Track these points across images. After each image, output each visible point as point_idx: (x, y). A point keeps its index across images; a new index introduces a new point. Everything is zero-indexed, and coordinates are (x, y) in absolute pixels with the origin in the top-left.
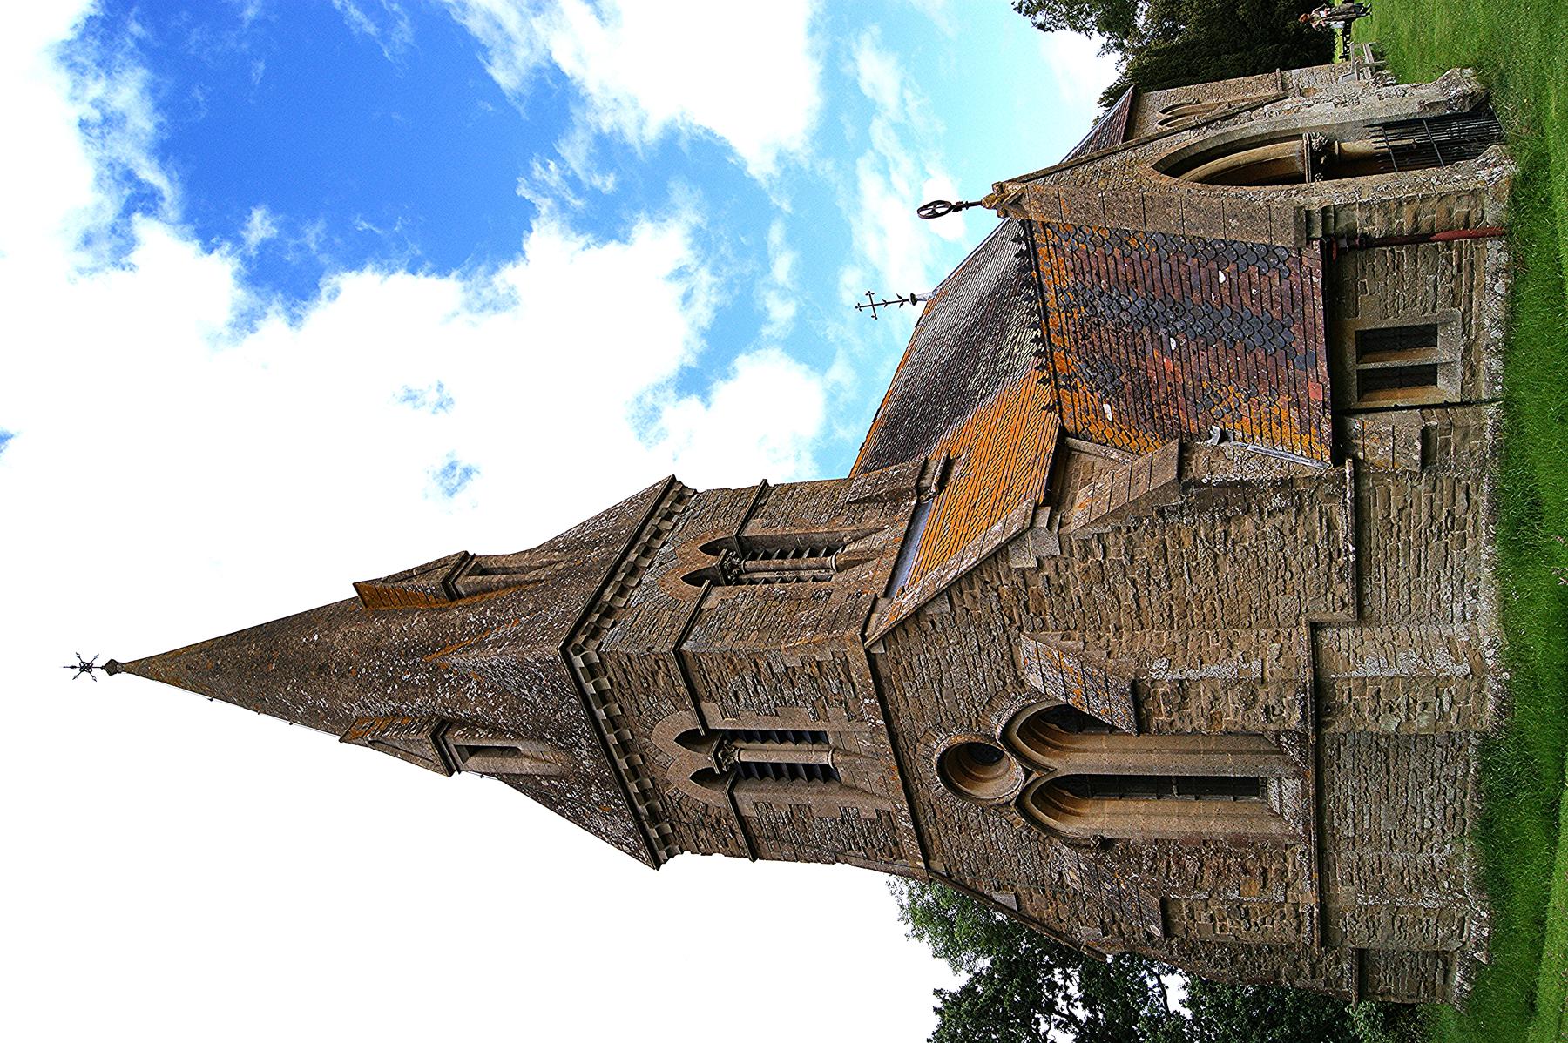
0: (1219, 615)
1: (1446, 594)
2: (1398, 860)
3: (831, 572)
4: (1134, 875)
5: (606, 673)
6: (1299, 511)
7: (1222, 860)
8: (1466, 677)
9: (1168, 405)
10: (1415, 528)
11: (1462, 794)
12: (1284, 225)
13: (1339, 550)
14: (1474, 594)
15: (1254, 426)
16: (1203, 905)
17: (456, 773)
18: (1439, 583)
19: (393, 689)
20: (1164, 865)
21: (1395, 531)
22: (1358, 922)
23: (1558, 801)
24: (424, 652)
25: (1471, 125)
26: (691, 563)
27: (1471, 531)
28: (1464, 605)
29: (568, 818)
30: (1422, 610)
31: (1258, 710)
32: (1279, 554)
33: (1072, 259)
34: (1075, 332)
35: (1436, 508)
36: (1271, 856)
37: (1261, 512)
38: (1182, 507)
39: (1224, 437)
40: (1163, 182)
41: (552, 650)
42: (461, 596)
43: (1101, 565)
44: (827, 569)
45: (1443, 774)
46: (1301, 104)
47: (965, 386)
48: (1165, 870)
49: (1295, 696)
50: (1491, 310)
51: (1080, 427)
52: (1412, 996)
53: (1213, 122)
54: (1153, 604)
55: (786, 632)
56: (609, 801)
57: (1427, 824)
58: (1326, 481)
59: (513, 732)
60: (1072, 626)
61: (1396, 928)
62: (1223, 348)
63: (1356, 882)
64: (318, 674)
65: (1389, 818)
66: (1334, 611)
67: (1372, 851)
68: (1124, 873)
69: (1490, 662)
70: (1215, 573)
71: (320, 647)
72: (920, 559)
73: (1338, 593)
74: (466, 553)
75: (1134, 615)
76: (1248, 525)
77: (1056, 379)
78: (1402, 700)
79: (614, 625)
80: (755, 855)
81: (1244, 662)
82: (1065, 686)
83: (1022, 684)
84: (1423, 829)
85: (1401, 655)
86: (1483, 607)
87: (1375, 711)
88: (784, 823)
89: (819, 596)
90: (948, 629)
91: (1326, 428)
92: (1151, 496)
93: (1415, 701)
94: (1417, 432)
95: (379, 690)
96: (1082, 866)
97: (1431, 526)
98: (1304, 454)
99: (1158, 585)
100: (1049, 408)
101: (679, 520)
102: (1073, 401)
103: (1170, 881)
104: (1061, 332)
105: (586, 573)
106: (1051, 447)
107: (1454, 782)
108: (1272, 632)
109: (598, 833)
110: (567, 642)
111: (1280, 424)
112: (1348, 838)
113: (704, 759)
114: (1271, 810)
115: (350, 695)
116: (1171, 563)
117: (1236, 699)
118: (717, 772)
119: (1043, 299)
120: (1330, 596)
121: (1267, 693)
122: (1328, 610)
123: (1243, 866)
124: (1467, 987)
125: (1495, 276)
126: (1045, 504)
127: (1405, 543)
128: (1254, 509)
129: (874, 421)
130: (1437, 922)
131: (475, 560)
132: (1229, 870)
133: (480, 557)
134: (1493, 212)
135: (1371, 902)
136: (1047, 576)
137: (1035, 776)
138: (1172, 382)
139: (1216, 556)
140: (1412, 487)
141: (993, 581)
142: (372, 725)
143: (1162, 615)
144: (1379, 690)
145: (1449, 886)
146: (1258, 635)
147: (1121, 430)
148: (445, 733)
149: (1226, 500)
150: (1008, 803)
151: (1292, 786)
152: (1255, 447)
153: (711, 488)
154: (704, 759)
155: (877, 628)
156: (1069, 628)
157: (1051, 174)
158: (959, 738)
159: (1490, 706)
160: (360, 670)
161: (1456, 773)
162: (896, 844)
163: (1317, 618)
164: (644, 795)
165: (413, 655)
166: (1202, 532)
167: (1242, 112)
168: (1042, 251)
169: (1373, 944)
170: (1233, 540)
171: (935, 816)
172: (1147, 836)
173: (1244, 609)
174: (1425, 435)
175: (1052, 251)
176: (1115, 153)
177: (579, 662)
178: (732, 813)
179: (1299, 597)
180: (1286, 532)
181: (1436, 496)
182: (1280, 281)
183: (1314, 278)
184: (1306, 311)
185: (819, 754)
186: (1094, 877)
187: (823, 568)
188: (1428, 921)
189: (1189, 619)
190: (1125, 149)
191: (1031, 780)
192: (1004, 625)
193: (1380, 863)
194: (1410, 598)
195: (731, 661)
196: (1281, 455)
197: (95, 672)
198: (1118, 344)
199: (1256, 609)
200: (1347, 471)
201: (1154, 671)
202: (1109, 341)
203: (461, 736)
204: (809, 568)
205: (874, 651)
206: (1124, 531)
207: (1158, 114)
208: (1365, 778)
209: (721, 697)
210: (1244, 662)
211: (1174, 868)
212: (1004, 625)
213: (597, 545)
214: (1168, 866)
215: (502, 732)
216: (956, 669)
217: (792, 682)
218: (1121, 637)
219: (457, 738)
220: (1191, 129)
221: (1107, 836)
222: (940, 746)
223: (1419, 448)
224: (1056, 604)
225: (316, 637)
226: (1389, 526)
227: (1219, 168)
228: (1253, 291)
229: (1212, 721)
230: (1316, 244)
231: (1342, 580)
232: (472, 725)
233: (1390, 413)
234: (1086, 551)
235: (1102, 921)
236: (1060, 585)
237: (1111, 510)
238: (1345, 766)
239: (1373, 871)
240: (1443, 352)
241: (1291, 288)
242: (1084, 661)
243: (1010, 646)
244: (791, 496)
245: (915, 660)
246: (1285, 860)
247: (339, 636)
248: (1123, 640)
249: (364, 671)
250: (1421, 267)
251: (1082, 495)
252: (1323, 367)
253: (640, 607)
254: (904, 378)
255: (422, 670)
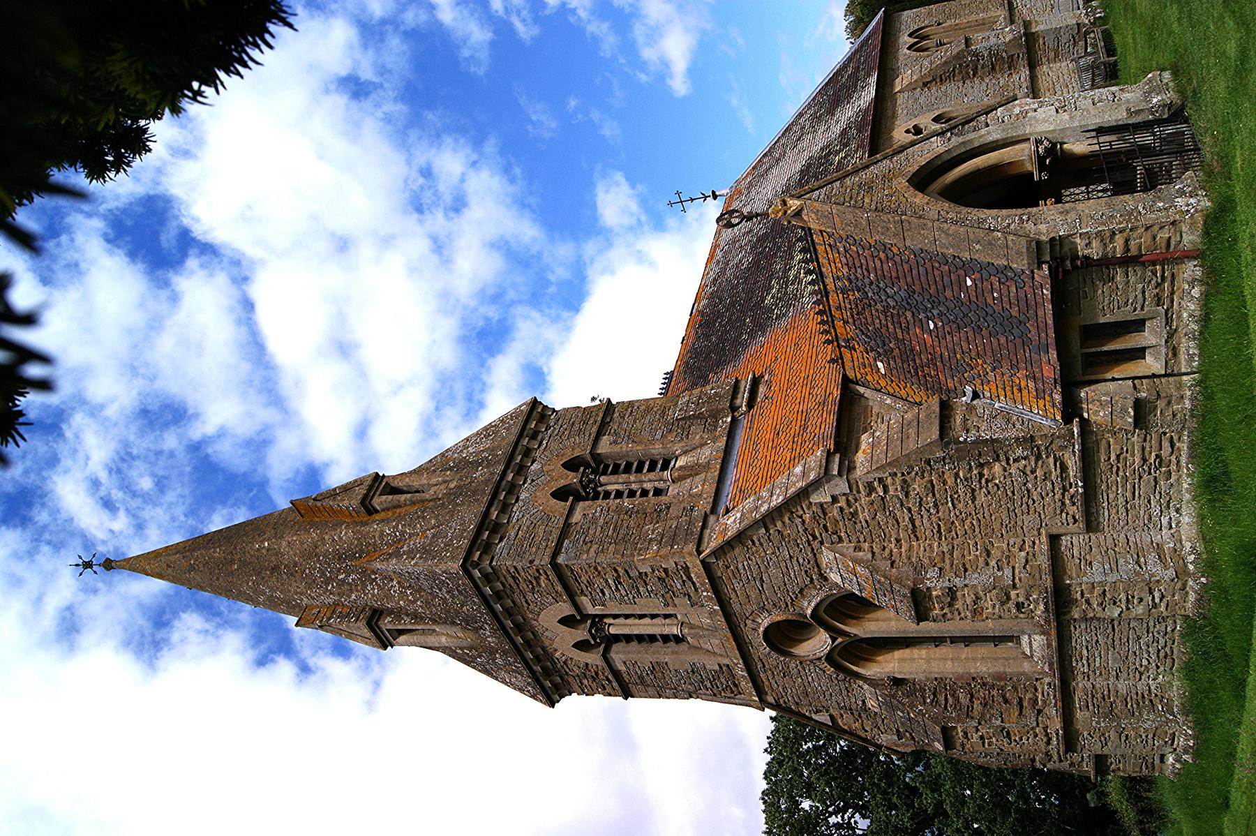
0: (977, 530)
1: (1156, 511)
2: (1122, 686)
3: (668, 483)
4: (920, 708)
5: (499, 578)
6: (1038, 457)
7: (987, 692)
8: (1172, 580)
9: (929, 367)
10: (1130, 467)
11: (1171, 642)
12: (1019, 253)
13: (1071, 484)
14: (1177, 511)
15: (999, 390)
16: (974, 730)
17: (389, 648)
18: (1150, 504)
19: (333, 587)
20: (943, 698)
21: (1114, 469)
22: (1093, 738)
23: (1244, 681)
24: (352, 557)
25: (1170, 130)
26: (556, 480)
27: (1175, 468)
28: (1170, 518)
29: (479, 671)
30: (1137, 522)
31: (1011, 605)
32: (1023, 488)
33: (846, 257)
34: (851, 309)
35: (1146, 454)
36: (1025, 688)
37: (1008, 459)
38: (944, 458)
39: (976, 395)
40: (917, 201)
41: (455, 566)
42: (377, 511)
43: (882, 498)
44: (665, 481)
45: (1156, 629)
46: (1027, 108)
47: (763, 301)
48: (943, 702)
49: (1039, 595)
50: (1188, 307)
51: (859, 376)
52: (1137, 772)
53: (955, 127)
54: (924, 524)
55: (637, 544)
56: (510, 664)
57: (1145, 662)
58: (1058, 437)
59: (430, 619)
60: (862, 539)
61: (1123, 740)
62: (972, 332)
63: (1091, 707)
64: (272, 574)
65: (1115, 660)
66: (1068, 524)
67: (1103, 681)
68: (912, 706)
69: (1191, 567)
70: (973, 502)
71: (270, 552)
72: (738, 476)
73: (1071, 513)
74: (377, 474)
75: (910, 532)
76: (997, 468)
77: (837, 341)
78: (1123, 596)
79: (501, 540)
80: (627, 694)
81: (998, 570)
82: (859, 585)
83: (826, 579)
84: (1141, 666)
85: (1121, 561)
86: (1186, 519)
87: (1102, 604)
88: (647, 674)
89: (661, 510)
90: (764, 545)
91: (1058, 397)
92: (919, 451)
93: (1133, 597)
94: (1130, 403)
95: (321, 587)
96: (880, 698)
97: (1143, 465)
98: (1040, 412)
99: (928, 511)
100: (832, 361)
101: (543, 439)
102: (852, 357)
103: (948, 711)
104: (839, 308)
105: (474, 492)
106: (837, 393)
107: (1166, 635)
108: (1019, 541)
109: (504, 682)
110: (466, 559)
111: (1020, 390)
112: (1084, 673)
113: (582, 634)
114: (1024, 653)
115: (299, 590)
116: (937, 496)
117: (993, 598)
118: (593, 642)
119: (823, 283)
120: (1064, 515)
121: (1018, 595)
122: (1063, 524)
123: (1004, 696)
124: (1178, 766)
125: (1192, 284)
126: (836, 451)
127: (1123, 477)
128: (1002, 457)
129: (691, 315)
130: (1154, 736)
131: (385, 480)
132: (993, 700)
133: (388, 476)
134: (1190, 238)
135: (1102, 724)
136: (840, 507)
137: (840, 640)
138: (932, 352)
139: (973, 491)
140: (1127, 439)
141: (797, 510)
142: (319, 612)
143: (932, 531)
144: (1105, 590)
145: (1163, 708)
146: (1008, 544)
147: (892, 381)
148: (378, 620)
149: (980, 452)
150: (820, 659)
151: (1038, 640)
152: (1001, 405)
153: (566, 407)
154: (582, 634)
155: (708, 543)
156: (860, 542)
157: (824, 186)
158: (778, 617)
159: (1192, 597)
160: (304, 571)
161: (1166, 629)
162: (735, 685)
163: (1054, 531)
164: (538, 659)
165: (345, 559)
166: (961, 474)
167: (979, 116)
168: (820, 249)
169: (1106, 751)
170: (986, 479)
171: (764, 666)
172: (928, 675)
173: (996, 526)
174: (1138, 404)
175: (828, 249)
176: (876, 163)
177: (477, 573)
178: (606, 668)
179: (1040, 516)
180: (1028, 473)
181: (1147, 445)
182: (1017, 290)
183: (1044, 291)
184: (1039, 313)
185: (670, 627)
186: (889, 705)
187: (662, 480)
188: (1147, 736)
189: (953, 533)
190: (884, 158)
191: (836, 643)
192: (808, 541)
193: (1109, 690)
194: (1127, 515)
195: (596, 569)
196: (1022, 413)
197: (95, 568)
198: (886, 320)
199: (1007, 525)
200: (1075, 429)
201: (928, 579)
202: (879, 318)
203: (390, 622)
204: (650, 481)
205: (708, 560)
206: (899, 475)
207: (906, 38)
208: (1096, 634)
209: (590, 593)
210: (998, 570)
211: (950, 700)
212: (808, 541)
213: (480, 465)
214: (946, 699)
215: (422, 618)
216: (772, 571)
217: (645, 582)
218: (901, 548)
219: (387, 623)
220: (937, 135)
221: (897, 676)
222: (765, 622)
223: (1132, 414)
224: (849, 526)
225: (266, 544)
226: (1110, 467)
227: (962, 173)
228: (995, 294)
229: (975, 613)
230: (1045, 267)
231: (1074, 504)
232: (398, 613)
233: (1108, 383)
234: (870, 489)
235: (898, 731)
236: (851, 513)
237: (888, 461)
238: (1080, 627)
239: (1103, 698)
240: (1150, 336)
241: (1026, 296)
242: (873, 570)
243: (815, 555)
244: (631, 414)
245: (740, 566)
246: (1036, 690)
247: (284, 543)
248: (903, 550)
249: (307, 571)
250: (1132, 279)
251: (865, 439)
252: (1053, 354)
253: (520, 523)
254: (712, 275)
255: (353, 572)
